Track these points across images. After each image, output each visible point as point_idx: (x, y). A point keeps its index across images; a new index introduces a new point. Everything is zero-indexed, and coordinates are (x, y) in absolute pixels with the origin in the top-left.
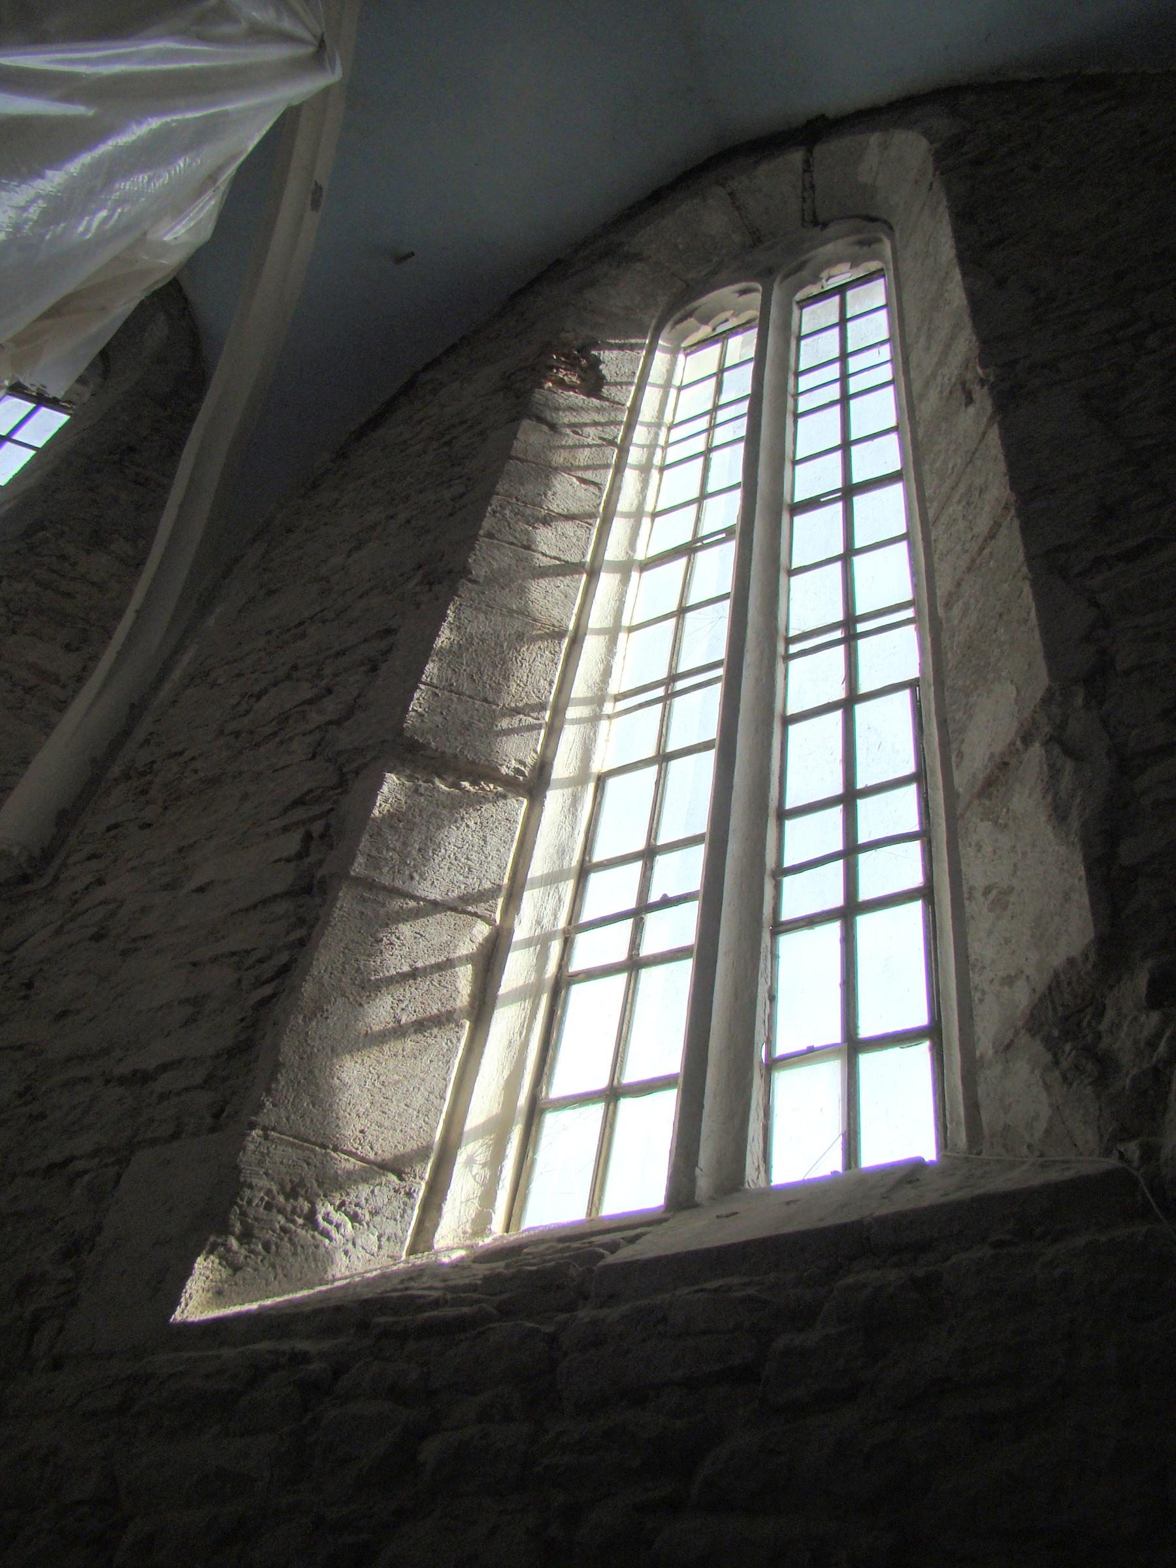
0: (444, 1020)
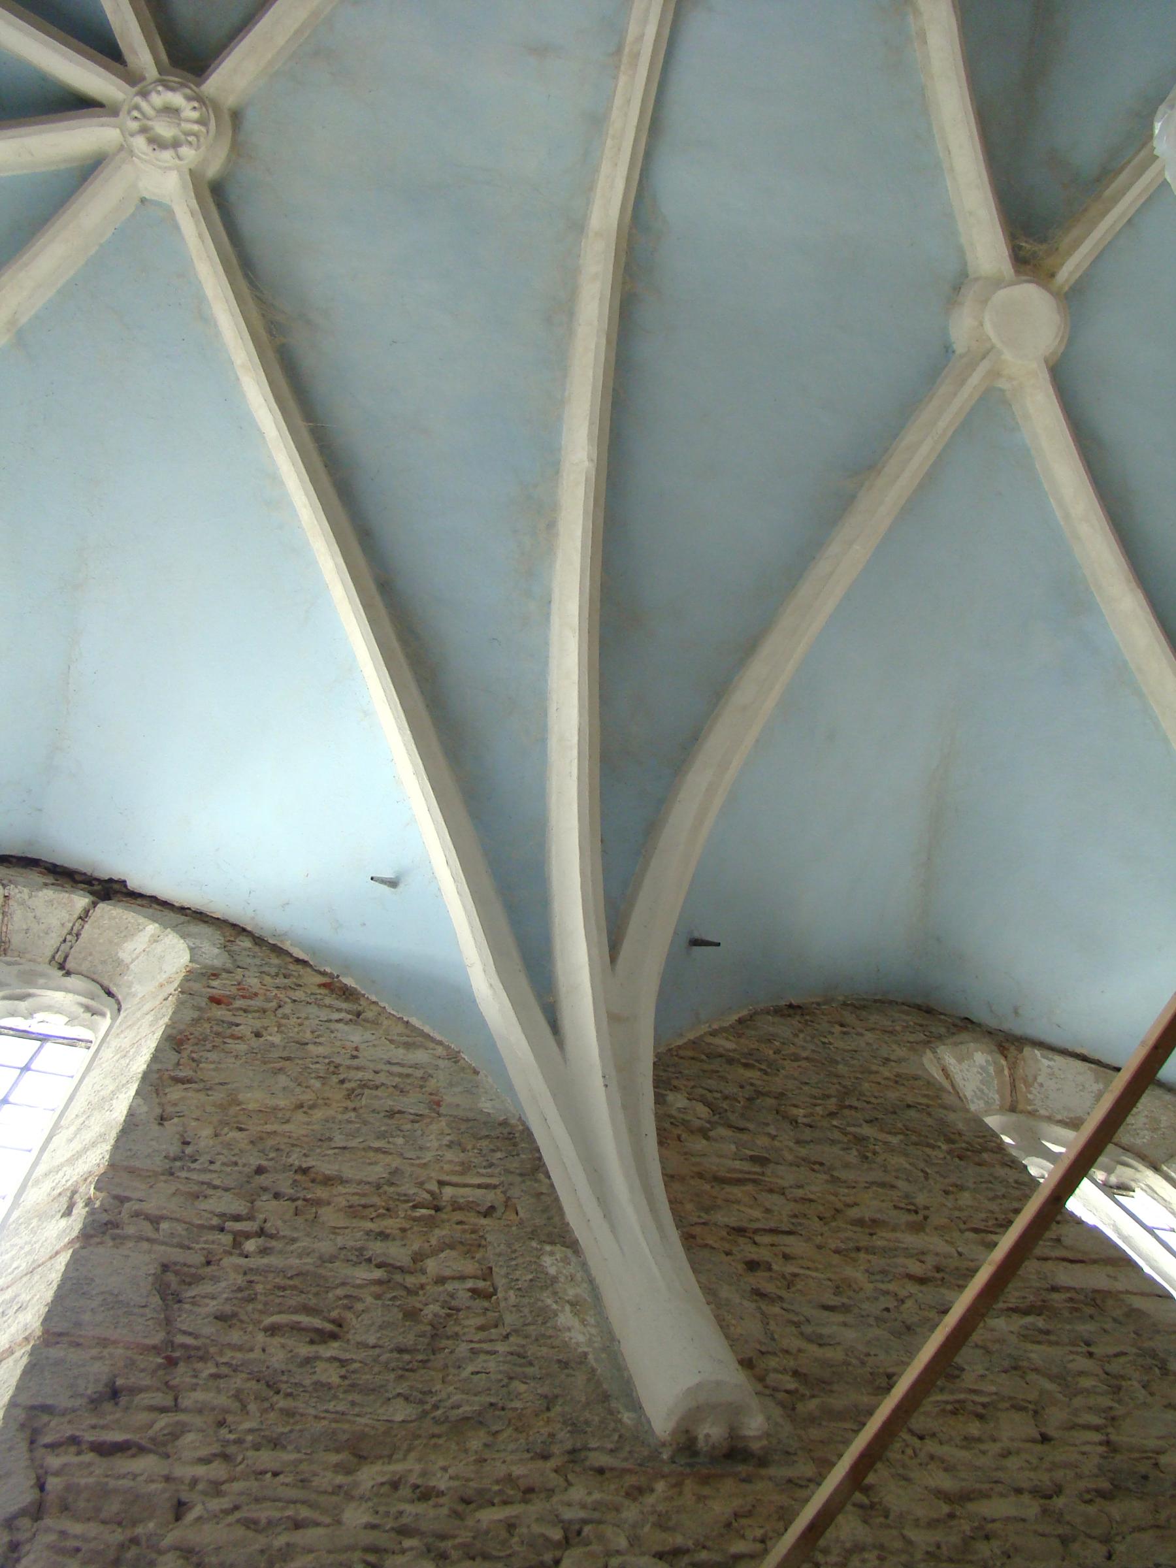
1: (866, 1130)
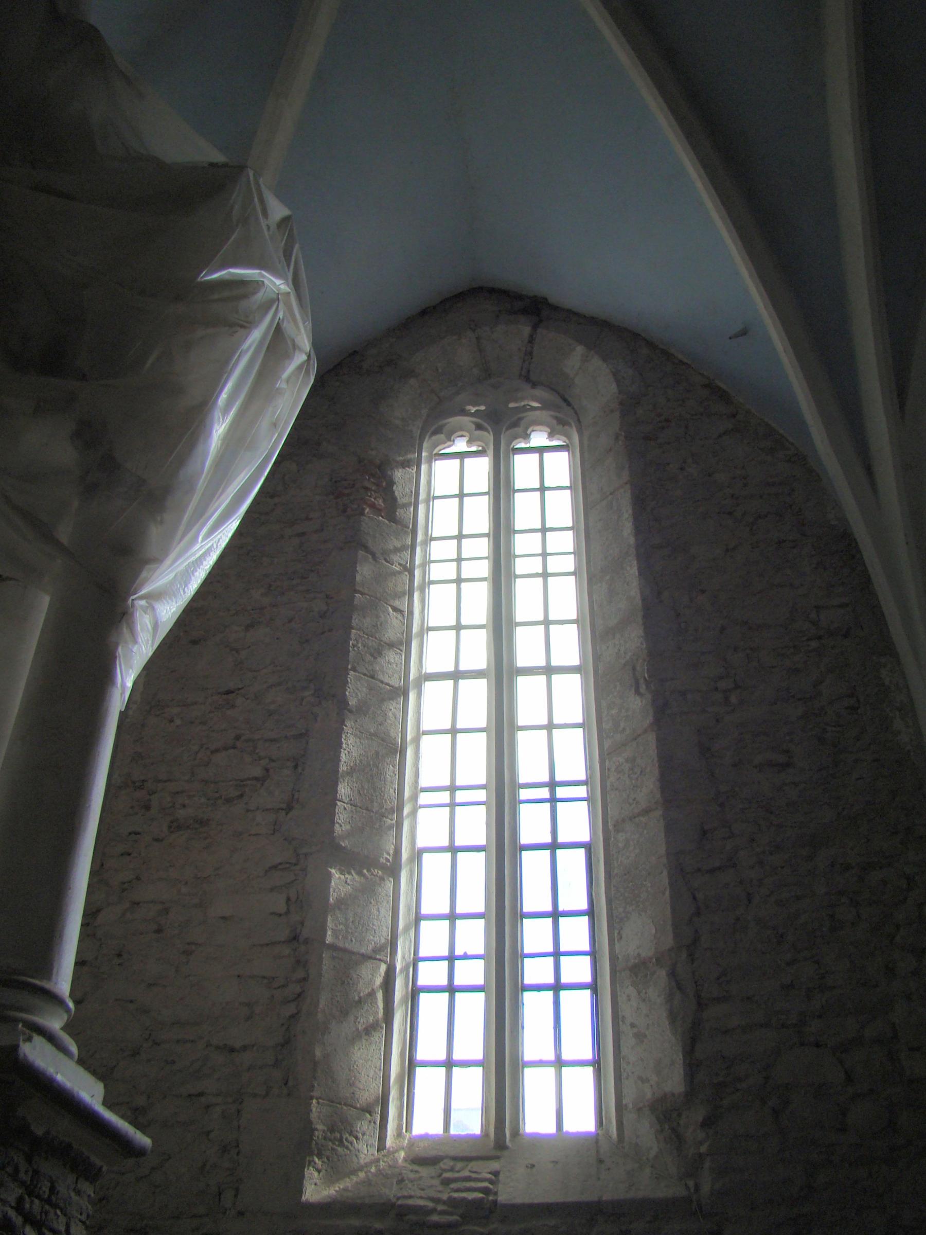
0: (374, 1027)
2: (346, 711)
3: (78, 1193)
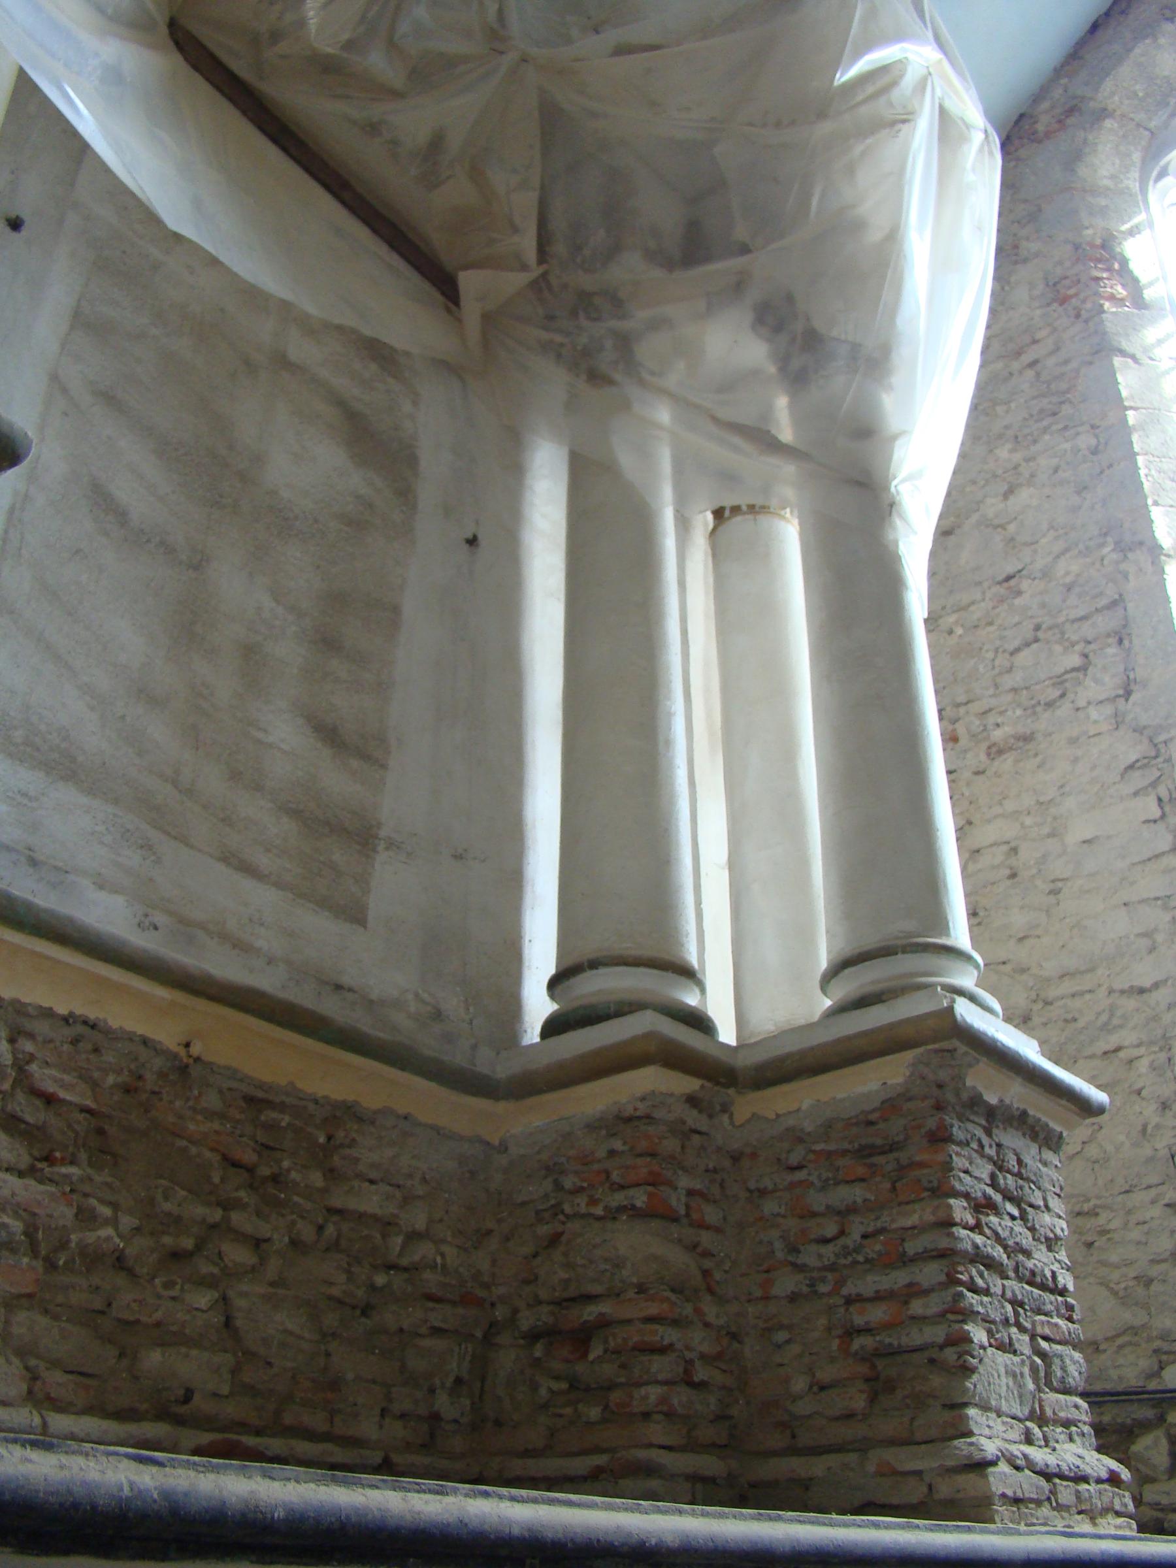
1: (801, 1175)
2: (1163, 558)
3: (1045, 1164)
